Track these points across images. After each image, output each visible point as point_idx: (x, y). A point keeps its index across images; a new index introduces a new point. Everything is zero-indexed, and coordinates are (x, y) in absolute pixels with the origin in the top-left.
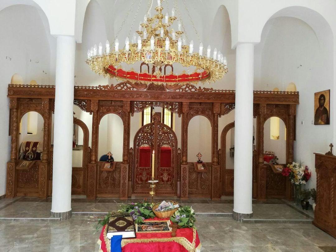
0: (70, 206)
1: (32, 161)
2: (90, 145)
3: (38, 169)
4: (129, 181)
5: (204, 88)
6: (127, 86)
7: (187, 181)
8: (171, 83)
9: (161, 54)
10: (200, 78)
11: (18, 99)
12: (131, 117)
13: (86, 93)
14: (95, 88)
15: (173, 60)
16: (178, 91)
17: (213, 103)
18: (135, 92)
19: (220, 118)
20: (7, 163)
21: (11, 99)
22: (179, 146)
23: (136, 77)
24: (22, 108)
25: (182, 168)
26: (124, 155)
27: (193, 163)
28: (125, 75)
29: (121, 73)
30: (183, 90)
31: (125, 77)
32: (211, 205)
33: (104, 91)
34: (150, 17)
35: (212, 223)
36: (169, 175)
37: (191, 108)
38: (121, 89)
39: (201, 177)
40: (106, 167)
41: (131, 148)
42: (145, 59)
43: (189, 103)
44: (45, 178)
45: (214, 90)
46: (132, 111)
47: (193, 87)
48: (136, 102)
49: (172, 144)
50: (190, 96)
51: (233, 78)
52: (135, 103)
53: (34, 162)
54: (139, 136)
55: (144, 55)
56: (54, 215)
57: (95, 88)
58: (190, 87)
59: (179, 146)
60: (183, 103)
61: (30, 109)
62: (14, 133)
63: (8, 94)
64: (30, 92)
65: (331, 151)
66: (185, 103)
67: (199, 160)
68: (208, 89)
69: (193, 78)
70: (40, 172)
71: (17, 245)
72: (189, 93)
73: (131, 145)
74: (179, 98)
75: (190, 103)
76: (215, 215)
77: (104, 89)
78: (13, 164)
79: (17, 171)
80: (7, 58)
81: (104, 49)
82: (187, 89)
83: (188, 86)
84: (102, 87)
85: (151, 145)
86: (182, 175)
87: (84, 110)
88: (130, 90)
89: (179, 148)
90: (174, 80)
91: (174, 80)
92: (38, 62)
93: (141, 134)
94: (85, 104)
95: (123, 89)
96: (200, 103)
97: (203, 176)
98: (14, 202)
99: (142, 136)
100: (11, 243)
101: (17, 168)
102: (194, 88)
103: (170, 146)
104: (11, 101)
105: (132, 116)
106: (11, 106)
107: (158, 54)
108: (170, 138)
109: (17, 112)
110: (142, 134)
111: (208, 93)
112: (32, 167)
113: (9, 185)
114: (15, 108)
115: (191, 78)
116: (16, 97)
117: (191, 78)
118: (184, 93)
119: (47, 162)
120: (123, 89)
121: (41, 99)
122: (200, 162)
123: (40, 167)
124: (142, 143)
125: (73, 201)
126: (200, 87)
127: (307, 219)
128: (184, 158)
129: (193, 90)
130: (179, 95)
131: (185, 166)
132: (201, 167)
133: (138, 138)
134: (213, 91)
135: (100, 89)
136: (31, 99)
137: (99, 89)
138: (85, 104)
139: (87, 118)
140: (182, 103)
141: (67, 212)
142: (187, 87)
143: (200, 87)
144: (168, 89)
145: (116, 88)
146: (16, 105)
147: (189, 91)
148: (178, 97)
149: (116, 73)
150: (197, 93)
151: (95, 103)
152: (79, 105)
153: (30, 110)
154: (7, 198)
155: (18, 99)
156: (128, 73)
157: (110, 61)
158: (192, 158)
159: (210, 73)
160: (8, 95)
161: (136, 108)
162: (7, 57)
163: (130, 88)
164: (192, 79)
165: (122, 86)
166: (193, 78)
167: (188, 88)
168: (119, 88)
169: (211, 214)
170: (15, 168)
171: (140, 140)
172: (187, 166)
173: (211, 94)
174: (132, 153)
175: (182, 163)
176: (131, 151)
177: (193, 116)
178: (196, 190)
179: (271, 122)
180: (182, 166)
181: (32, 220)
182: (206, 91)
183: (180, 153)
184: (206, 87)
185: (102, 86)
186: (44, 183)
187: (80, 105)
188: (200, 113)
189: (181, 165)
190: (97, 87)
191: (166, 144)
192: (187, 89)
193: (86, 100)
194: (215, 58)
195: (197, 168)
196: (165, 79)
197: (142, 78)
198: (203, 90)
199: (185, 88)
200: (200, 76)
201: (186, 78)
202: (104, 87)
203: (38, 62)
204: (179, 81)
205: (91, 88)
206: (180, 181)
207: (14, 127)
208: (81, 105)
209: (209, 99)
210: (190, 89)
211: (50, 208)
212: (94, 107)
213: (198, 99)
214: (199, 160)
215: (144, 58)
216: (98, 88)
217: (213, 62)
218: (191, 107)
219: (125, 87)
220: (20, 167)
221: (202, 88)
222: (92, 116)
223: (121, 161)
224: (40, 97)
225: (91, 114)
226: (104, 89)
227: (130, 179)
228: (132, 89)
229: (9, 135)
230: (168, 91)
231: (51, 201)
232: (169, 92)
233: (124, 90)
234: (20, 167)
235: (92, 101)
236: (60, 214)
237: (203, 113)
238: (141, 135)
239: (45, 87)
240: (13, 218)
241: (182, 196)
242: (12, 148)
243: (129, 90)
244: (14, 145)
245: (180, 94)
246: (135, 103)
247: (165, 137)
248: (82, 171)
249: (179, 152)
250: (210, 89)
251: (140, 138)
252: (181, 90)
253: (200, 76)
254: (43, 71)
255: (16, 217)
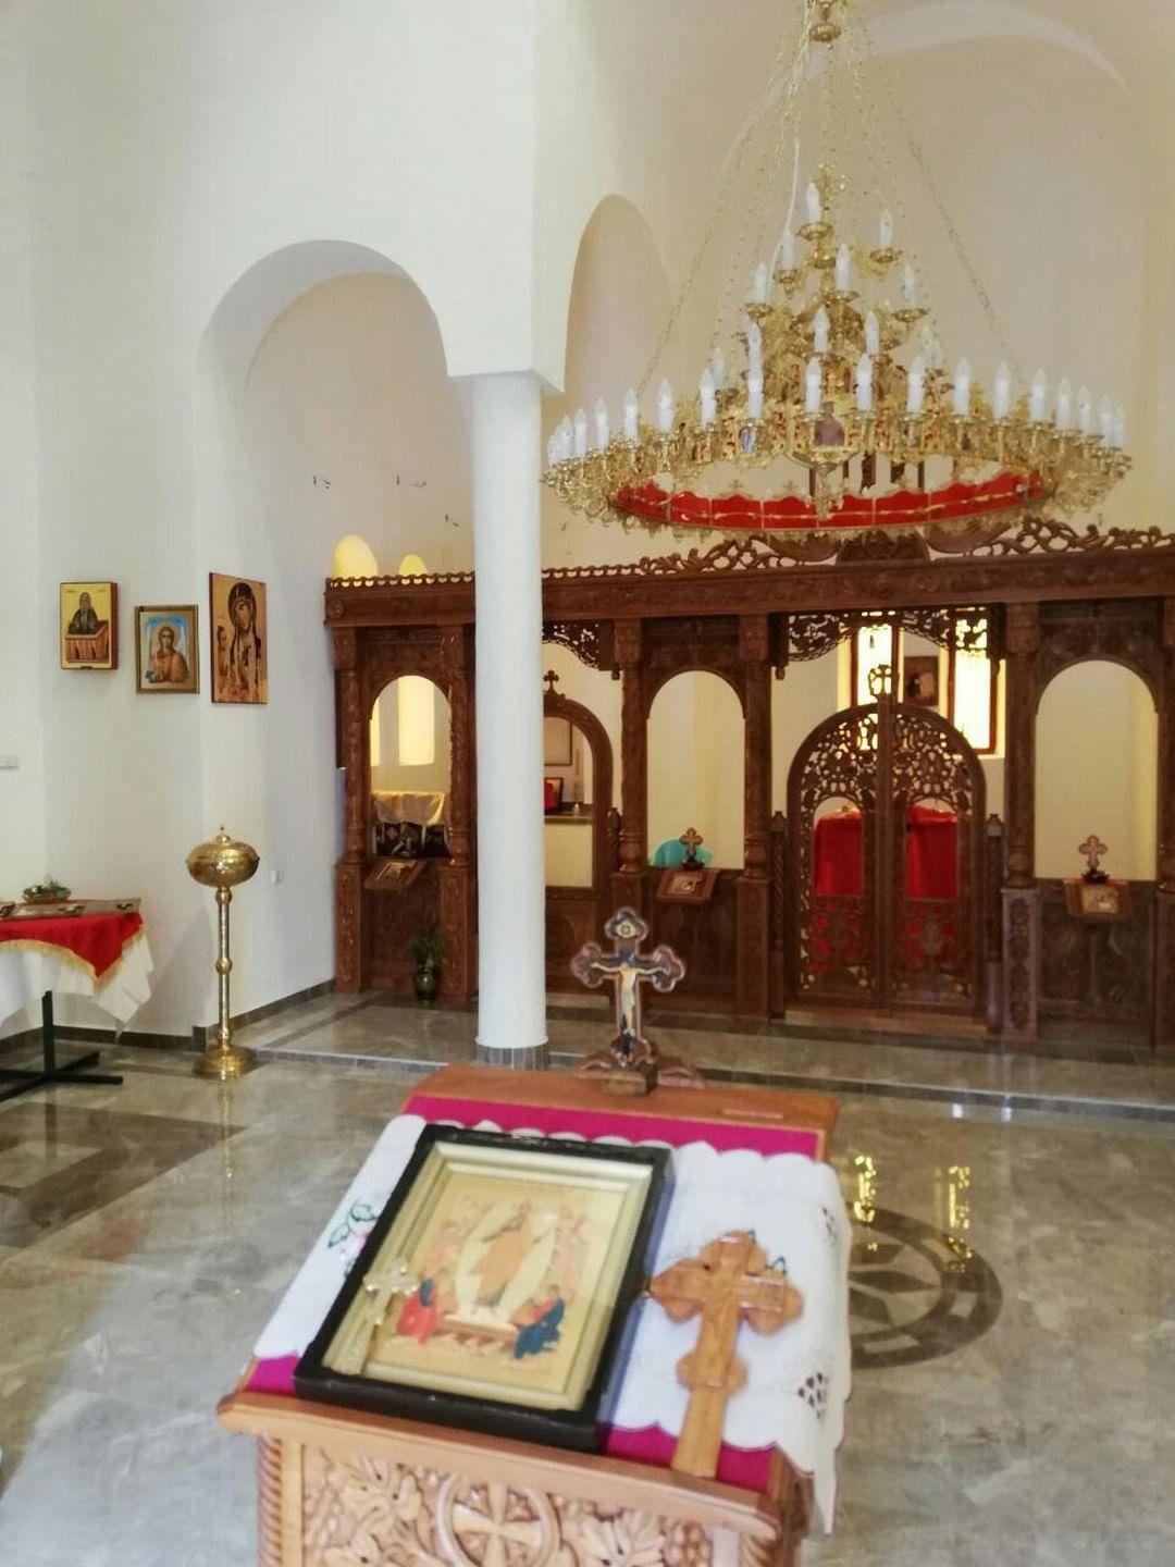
0: (544, 1031)
1: (414, 862)
2: (617, 801)
3: (438, 889)
4: (772, 947)
5: (1115, 532)
6: (754, 553)
7: (1031, 965)
8: (901, 525)
9: (797, 427)
10: (1021, 495)
11: (362, 634)
12: (775, 684)
13: (591, 594)
14: (614, 572)
15: (850, 444)
16: (982, 552)
17: (1160, 600)
18: (789, 572)
19: (780, 682)
20: (337, 867)
21: (336, 633)
22: (996, 803)
23: (751, 517)
24: (375, 663)
25: (1006, 902)
26: (749, 844)
27: (1058, 884)
28: (704, 516)
29: (689, 511)
30: (1006, 550)
31: (706, 521)
32: (1141, 1072)
33: (666, 579)
34: (788, 264)
35: (1127, 1146)
36: (947, 929)
37: (1048, 631)
38: (729, 568)
39: (1105, 950)
40: (676, 889)
41: (779, 813)
42: (738, 452)
43: (1036, 609)
44: (460, 924)
45: (1165, 538)
46: (779, 658)
47: (1056, 529)
48: (797, 619)
49: (961, 797)
50: (1041, 574)
51: (460, 522)
52: (792, 619)
53: (422, 864)
54: (811, 764)
55: (733, 440)
56: (487, 1052)
57: (629, 571)
58: (1045, 533)
59: (996, 803)
60: (1009, 610)
61: (402, 668)
62: (354, 756)
63: (327, 616)
64: (396, 604)
65: (571, 728)
66: (1019, 609)
67: (1093, 871)
68: (1134, 536)
69: (996, 496)
70: (442, 905)
71: (364, 1138)
72: (1038, 559)
73: (779, 802)
74: (990, 587)
75: (1042, 603)
76: (1149, 1115)
77: (660, 572)
78: (355, 871)
79: (369, 898)
80: (315, 482)
81: (592, 431)
82: (1029, 542)
83: (1034, 526)
84: (653, 566)
85: (862, 802)
86: (1006, 937)
87: (591, 662)
88: (766, 564)
89: (994, 816)
90: (910, 512)
91: (910, 512)
92: (424, 484)
93: (820, 755)
94: (592, 638)
95: (739, 566)
96: (1097, 602)
97: (1112, 943)
98: (364, 1005)
99: (823, 763)
100: (348, 1132)
101: (367, 885)
102: (1063, 537)
103: (952, 804)
104: (338, 638)
105: (780, 676)
106: (339, 657)
107: (784, 428)
108: (949, 771)
109: (359, 680)
110: (824, 756)
111: (1136, 554)
112: (415, 884)
113: (345, 944)
114: (352, 665)
115: (985, 498)
116: (352, 625)
117: (985, 498)
118: (1012, 561)
119: (466, 863)
120: (739, 566)
121: (433, 627)
122: (1095, 878)
123: (441, 885)
124: (823, 793)
125: (552, 1013)
126: (1092, 529)
127: (1027, 986)
128: (1015, 861)
129: (1058, 544)
130: (988, 571)
131: (1018, 894)
132: (1100, 903)
133: (808, 769)
134: (1161, 543)
135: (650, 574)
136: (404, 631)
137: (642, 573)
138: (592, 638)
139: (602, 694)
140: (1002, 606)
141: (529, 1050)
142: (1027, 531)
143: (1092, 529)
144: (934, 548)
145: (711, 565)
146: (353, 655)
147: (1038, 550)
148: (984, 580)
149: (668, 512)
150: (1078, 557)
151: (629, 631)
152: (572, 645)
153: (401, 671)
154: (341, 991)
155: (362, 634)
156: (719, 505)
157: (627, 476)
158: (1056, 858)
159: (1035, 475)
160: (328, 620)
161: (796, 642)
162: (314, 477)
163: (765, 558)
164: (991, 501)
165: (733, 552)
166: (996, 496)
167: (1035, 534)
168: (722, 563)
169: (1128, 1109)
170: (362, 886)
171: (814, 779)
172: (1028, 895)
173: (1151, 556)
174: (782, 833)
175: (1009, 883)
176: (776, 828)
177: (1060, 664)
178: (1075, 1002)
179: (400, 685)
180: (1009, 895)
181: (415, 1066)
182: (1123, 543)
183: (998, 839)
184: (1125, 525)
185: (654, 561)
186: (459, 942)
187: (576, 643)
188: (1095, 649)
189: (1003, 891)
190: (633, 567)
191: (932, 795)
192: (1029, 542)
193: (596, 622)
194: (1037, 413)
195: (1080, 905)
196: (874, 513)
197: (778, 517)
198: (1111, 539)
199: (1020, 538)
200: (1019, 489)
201: (964, 502)
202: (661, 562)
203: (424, 484)
204: (937, 514)
205: (625, 572)
206: (1000, 959)
207: (353, 735)
208: (580, 644)
209: (1140, 581)
210: (1044, 542)
211: (475, 1033)
212: (627, 646)
213: (1085, 583)
214: (1093, 871)
215: (734, 452)
216: (638, 571)
217: (1029, 432)
218: (1048, 622)
219: (747, 558)
220: (377, 881)
221: (1103, 531)
222: (619, 684)
223: (740, 865)
224: (429, 621)
225: (616, 677)
226: (660, 572)
227: (779, 942)
228: (773, 562)
229: (339, 765)
230: (934, 555)
231: (477, 1012)
232: (939, 564)
233: (743, 568)
234: (377, 881)
235: (618, 625)
236: (507, 1052)
237: (1112, 649)
238: (819, 759)
239: (449, 582)
240: (357, 1057)
241: (1008, 1024)
242: (348, 811)
243: (761, 566)
244: (356, 800)
245: (994, 567)
246: (792, 619)
247: (925, 767)
248: (593, 903)
249: (993, 831)
250: (1142, 533)
251: (812, 773)
252: (998, 550)
253: (1019, 489)
254: (447, 518)
255: (367, 1054)
